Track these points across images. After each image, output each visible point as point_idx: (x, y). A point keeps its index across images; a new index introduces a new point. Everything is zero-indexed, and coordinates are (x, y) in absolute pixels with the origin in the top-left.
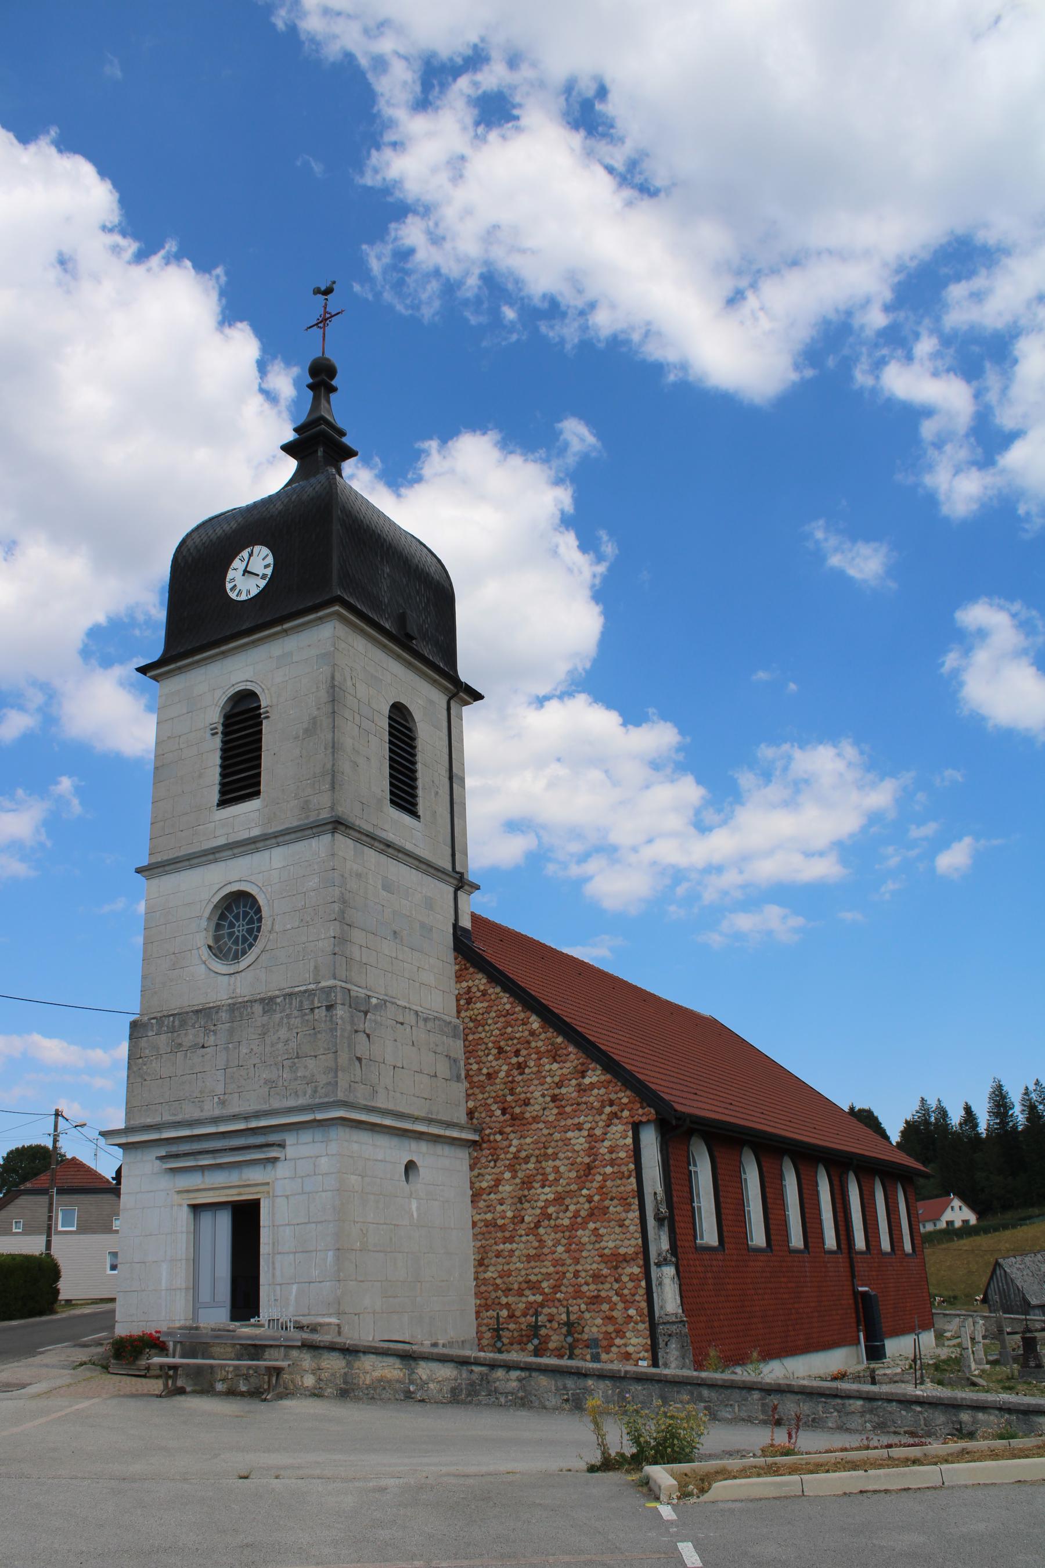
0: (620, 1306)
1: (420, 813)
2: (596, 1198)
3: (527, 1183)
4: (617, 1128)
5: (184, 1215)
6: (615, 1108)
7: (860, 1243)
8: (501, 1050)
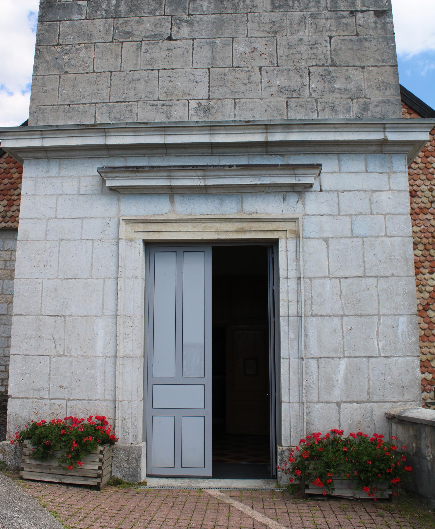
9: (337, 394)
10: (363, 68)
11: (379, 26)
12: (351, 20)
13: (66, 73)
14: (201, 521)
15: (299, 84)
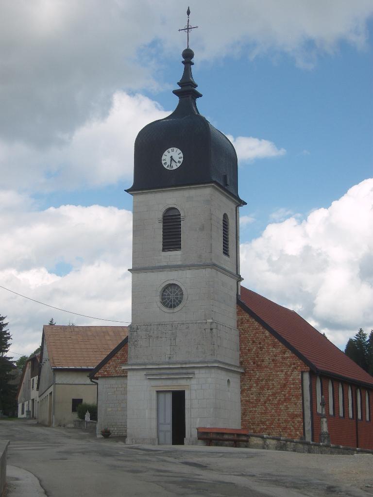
0: (294, 431)
1: (230, 254)
2: (287, 395)
3: (262, 388)
4: (296, 373)
5: (155, 394)
6: (295, 366)
7: (359, 417)
8: (254, 342)
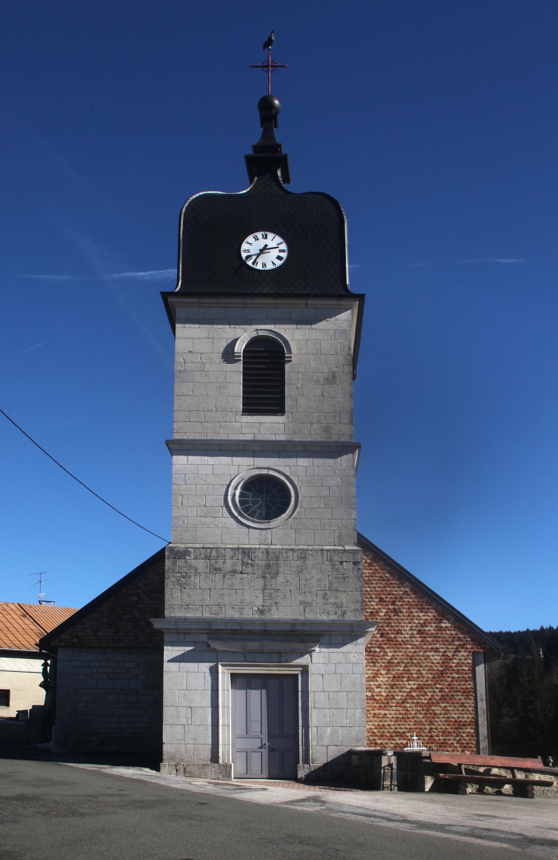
8: (381, 600)
9: (326, 742)
10: (345, 592)
11: (355, 570)
12: (340, 567)
13: (185, 588)
14: (317, 553)
15: (311, 599)
